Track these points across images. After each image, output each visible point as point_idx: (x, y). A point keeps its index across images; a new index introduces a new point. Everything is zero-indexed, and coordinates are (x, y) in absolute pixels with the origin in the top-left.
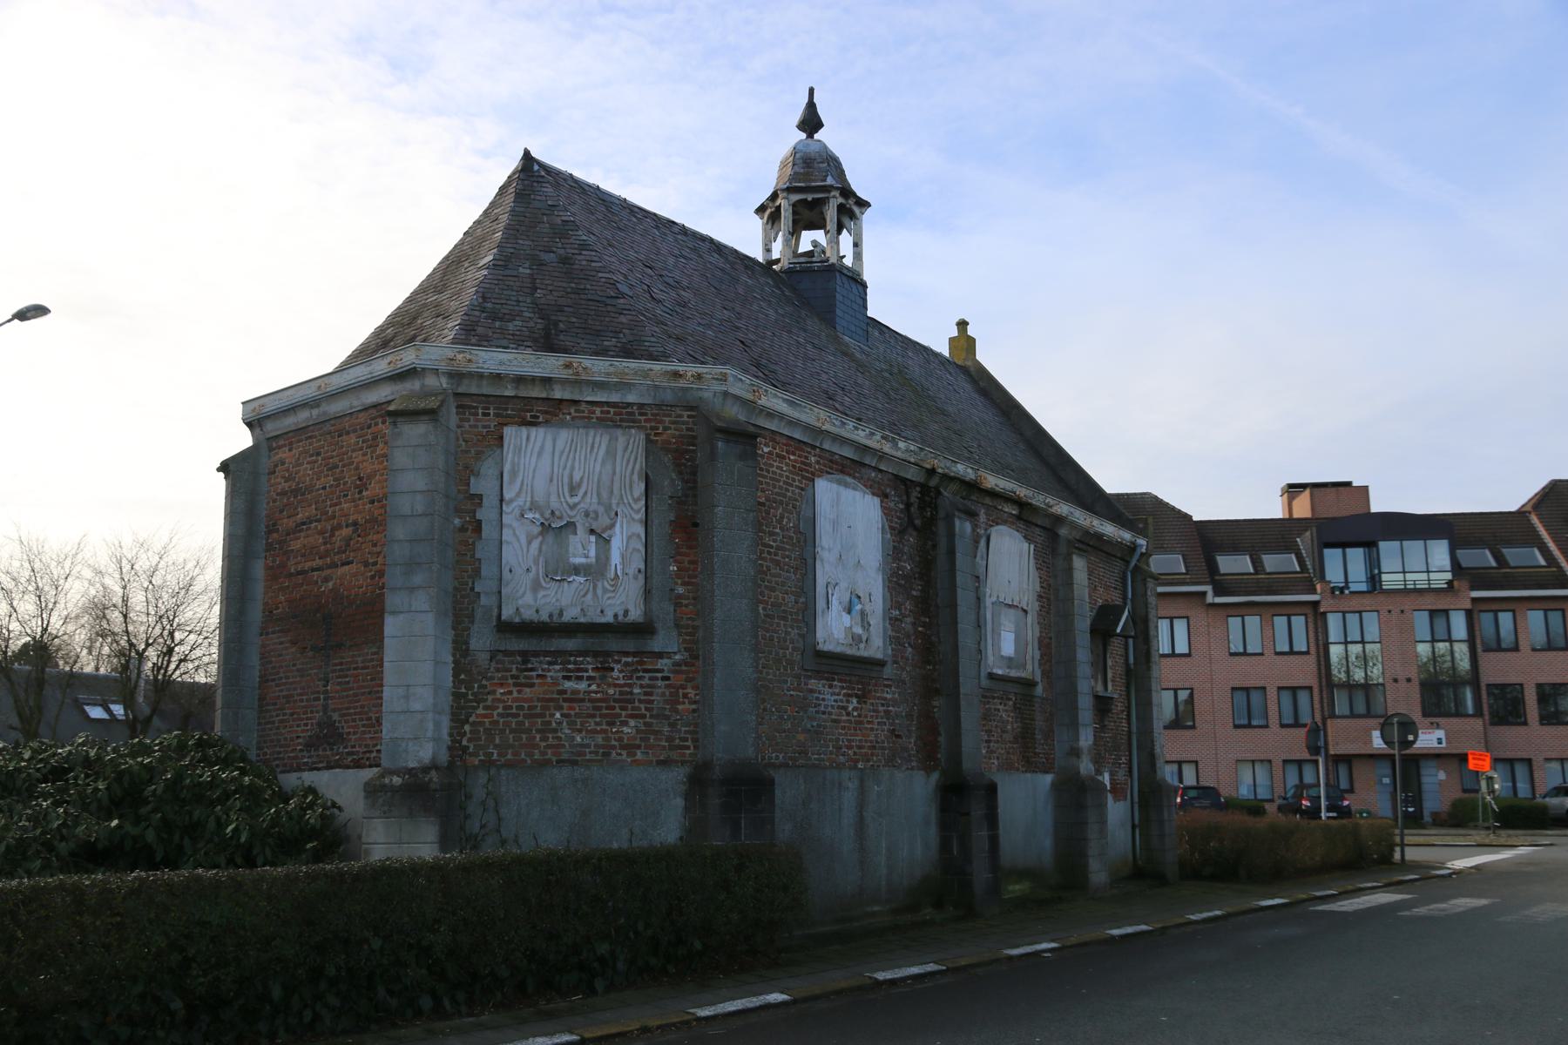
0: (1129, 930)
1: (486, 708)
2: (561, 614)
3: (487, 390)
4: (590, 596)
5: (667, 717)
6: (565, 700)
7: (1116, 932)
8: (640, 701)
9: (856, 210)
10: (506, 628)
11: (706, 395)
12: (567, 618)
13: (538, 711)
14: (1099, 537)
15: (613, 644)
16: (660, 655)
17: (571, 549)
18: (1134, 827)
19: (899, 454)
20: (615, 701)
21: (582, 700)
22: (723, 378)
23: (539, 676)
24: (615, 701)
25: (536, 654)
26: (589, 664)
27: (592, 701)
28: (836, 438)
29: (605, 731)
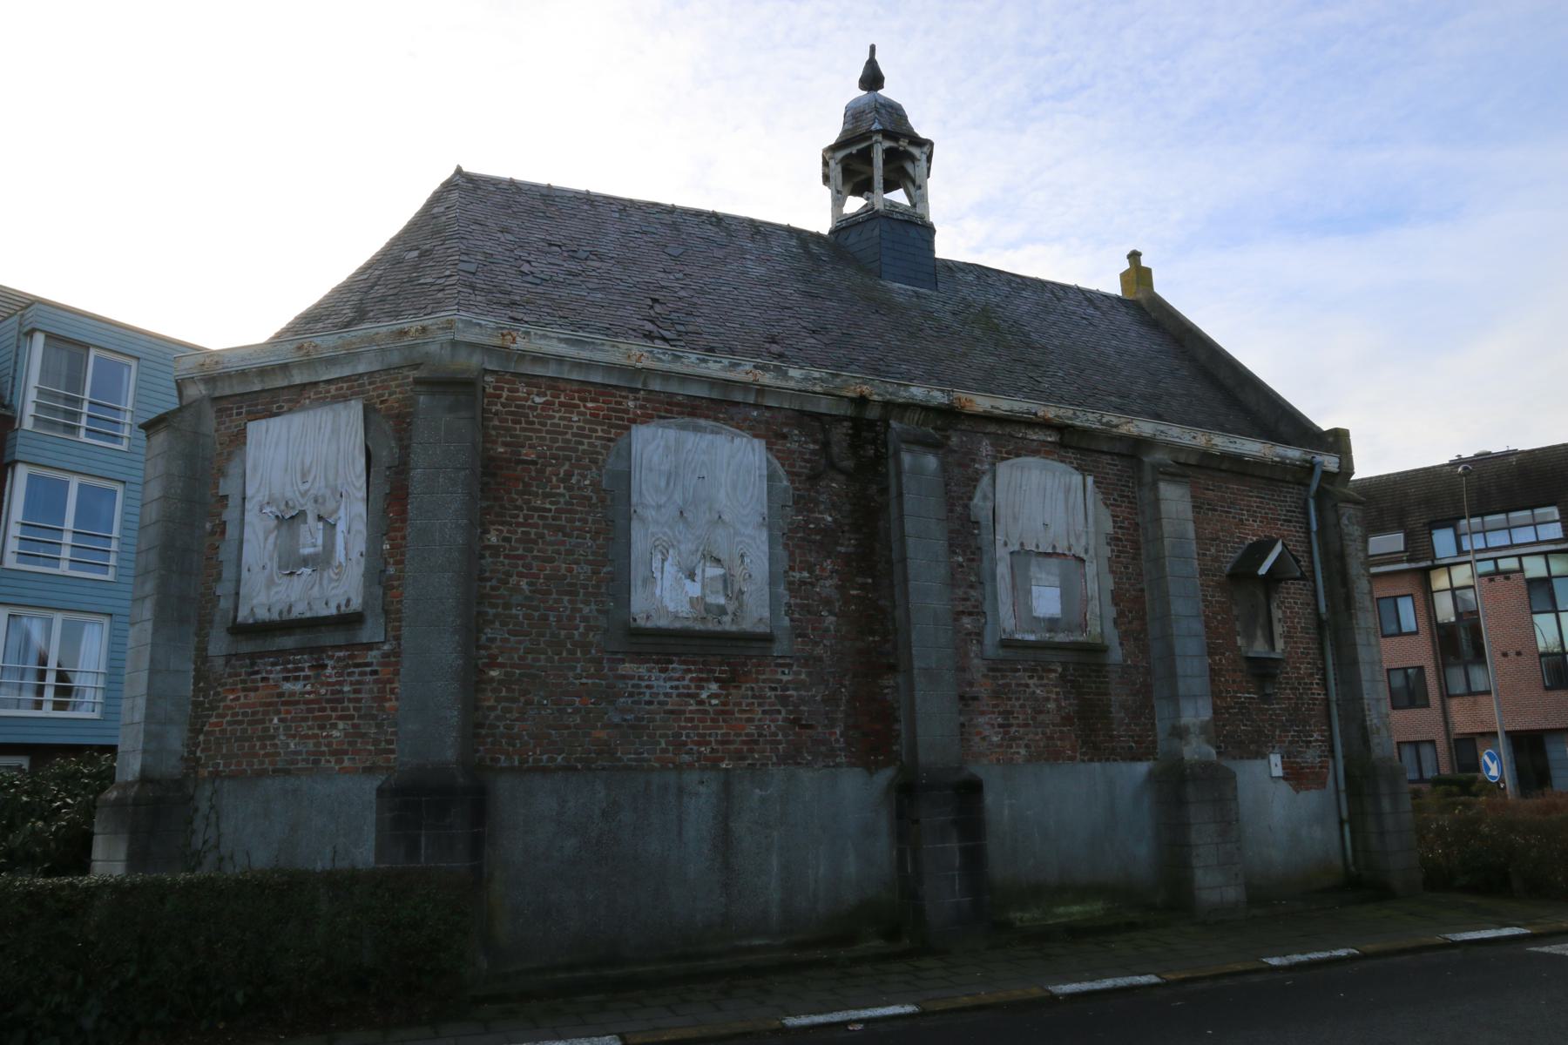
0: (1108, 983)
1: (219, 716)
2: (289, 611)
3: (238, 389)
4: (316, 588)
5: (374, 717)
6: (284, 703)
7: (1275, 961)
8: (350, 700)
9: (915, 151)
10: (240, 631)
11: (433, 348)
12: (295, 614)
13: (260, 716)
14: (1237, 459)
15: (327, 638)
16: (369, 646)
17: (302, 540)
18: (1341, 823)
19: (792, 384)
20: (328, 701)
21: (297, 703)
22: (449, 326)
23: (263, 679)
24: (328, 701)
25: (262, 655)
26: (306, 661)
27: (307, 702)
28: (667, 376)
29: (315, 736)
